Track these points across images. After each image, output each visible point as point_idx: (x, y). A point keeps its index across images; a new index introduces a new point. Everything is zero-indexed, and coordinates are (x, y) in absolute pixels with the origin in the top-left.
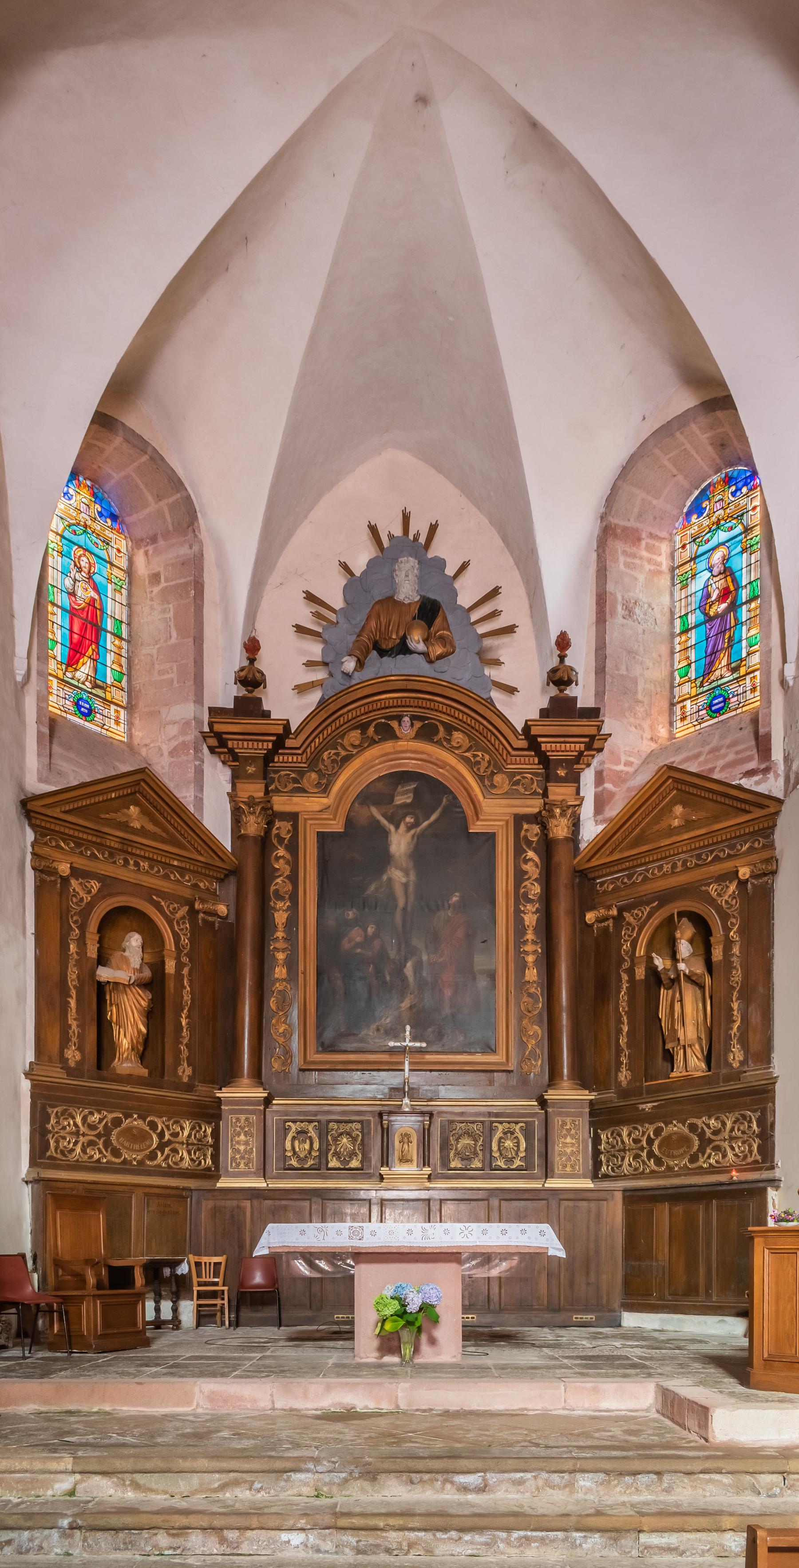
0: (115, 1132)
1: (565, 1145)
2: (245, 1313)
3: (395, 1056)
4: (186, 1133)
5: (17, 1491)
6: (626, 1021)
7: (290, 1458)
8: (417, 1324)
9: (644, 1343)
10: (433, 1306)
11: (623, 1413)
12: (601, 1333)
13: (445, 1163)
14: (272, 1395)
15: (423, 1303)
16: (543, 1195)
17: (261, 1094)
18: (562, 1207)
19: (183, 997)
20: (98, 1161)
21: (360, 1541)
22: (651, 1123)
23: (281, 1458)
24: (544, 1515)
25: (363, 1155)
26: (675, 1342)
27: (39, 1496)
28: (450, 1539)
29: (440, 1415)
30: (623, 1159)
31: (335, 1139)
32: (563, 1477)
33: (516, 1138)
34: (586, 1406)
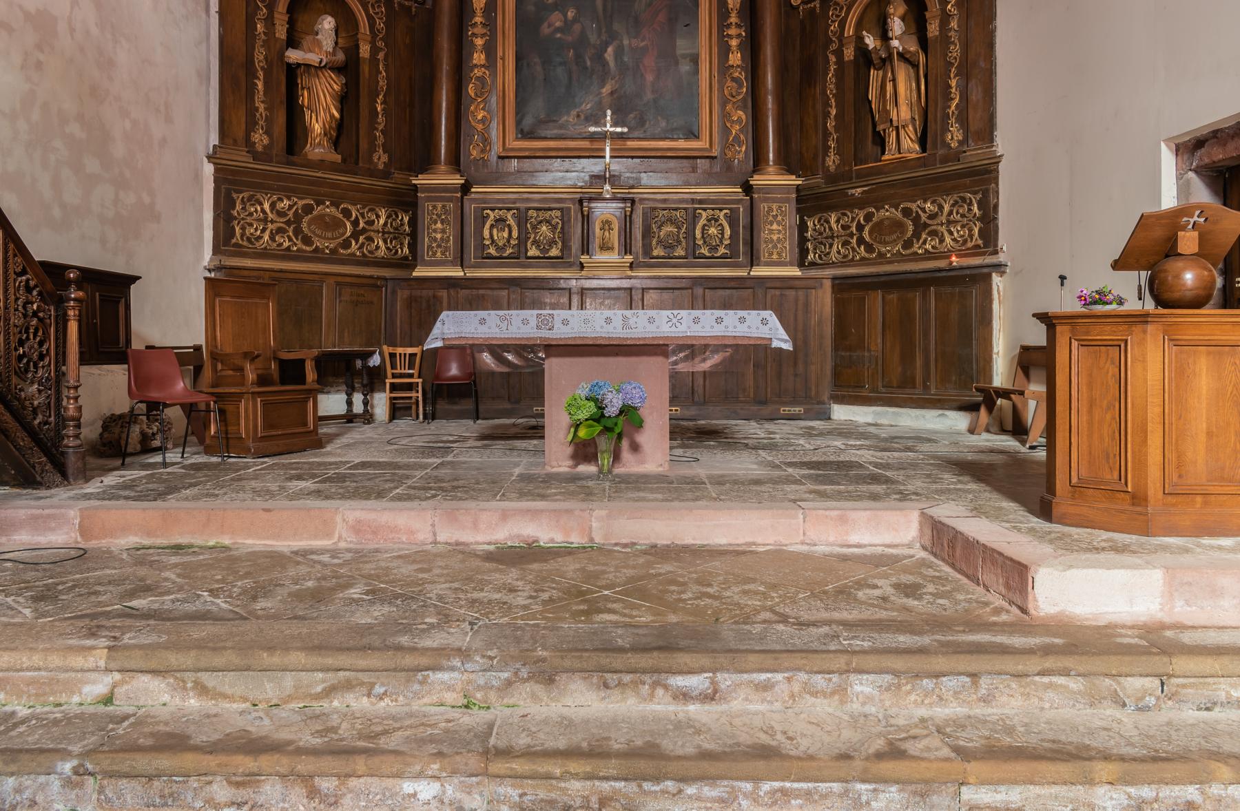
0: (306, 219)
1: (771, 231)
2: (442, 405)
3: (596, 143)
4: (382, 221)
5: (29, 696)
6: (834, 104)
7: (427, 649)
8: (617, 430)
9: (867, 443)
10: (636, 409)
11: (879, 550)
12: (812, 428)
13: (647, 250)
14: (433, 525)
15: (624, 405)
16: (748, 283)
17: (458, 180)
18: (769, 296)
19: (378, 82)
20: (288, 249)
21: (525, 794)
22: (861, 209)
23: (413, 649)
24: (811, 758)
25: (563, 243)
26: (901, 441)
27: (60, 705)
28: (663, 792)
29: (645, 553)
30: (831, 246)
31: (534, 227)
32: (830, 680)
33: (721, 225)
34: (831, 539)
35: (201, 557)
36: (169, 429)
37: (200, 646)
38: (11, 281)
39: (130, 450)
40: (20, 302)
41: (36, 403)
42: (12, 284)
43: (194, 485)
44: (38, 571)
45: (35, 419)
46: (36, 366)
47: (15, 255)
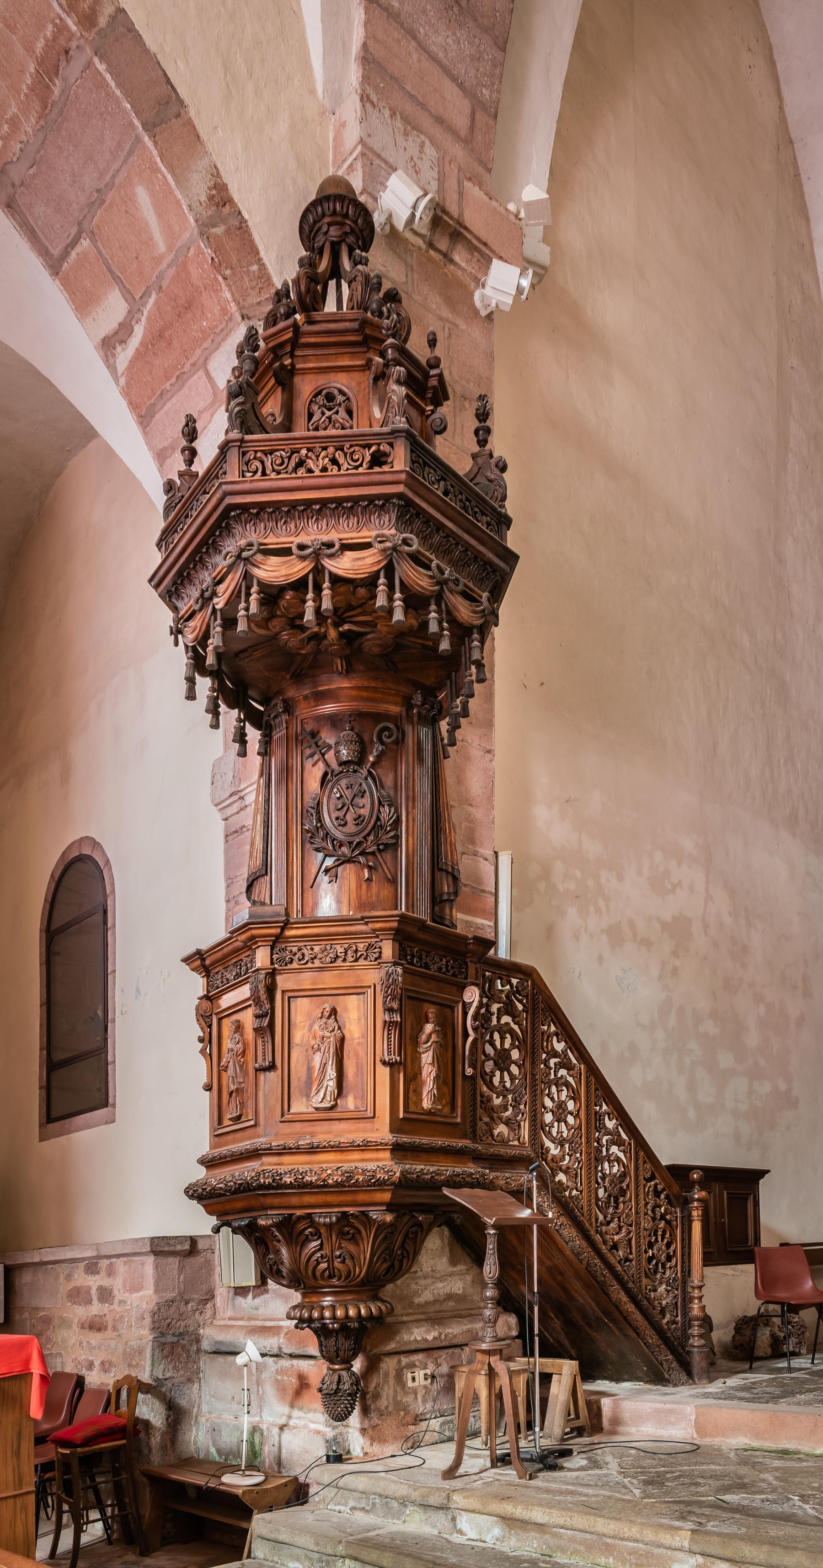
35: (805, 1464)
36: (803, 1333)
37: (773, 1543)
38: (641, 1187)
39: (759, 1352)
40: (649, 1207)
41: (664, 1303)
42: (642, 1190)
43: (810, 1391)
44: (654, 1459)
45: (664, 1318)
46: (664, 1267)
47: (645, 1162)
